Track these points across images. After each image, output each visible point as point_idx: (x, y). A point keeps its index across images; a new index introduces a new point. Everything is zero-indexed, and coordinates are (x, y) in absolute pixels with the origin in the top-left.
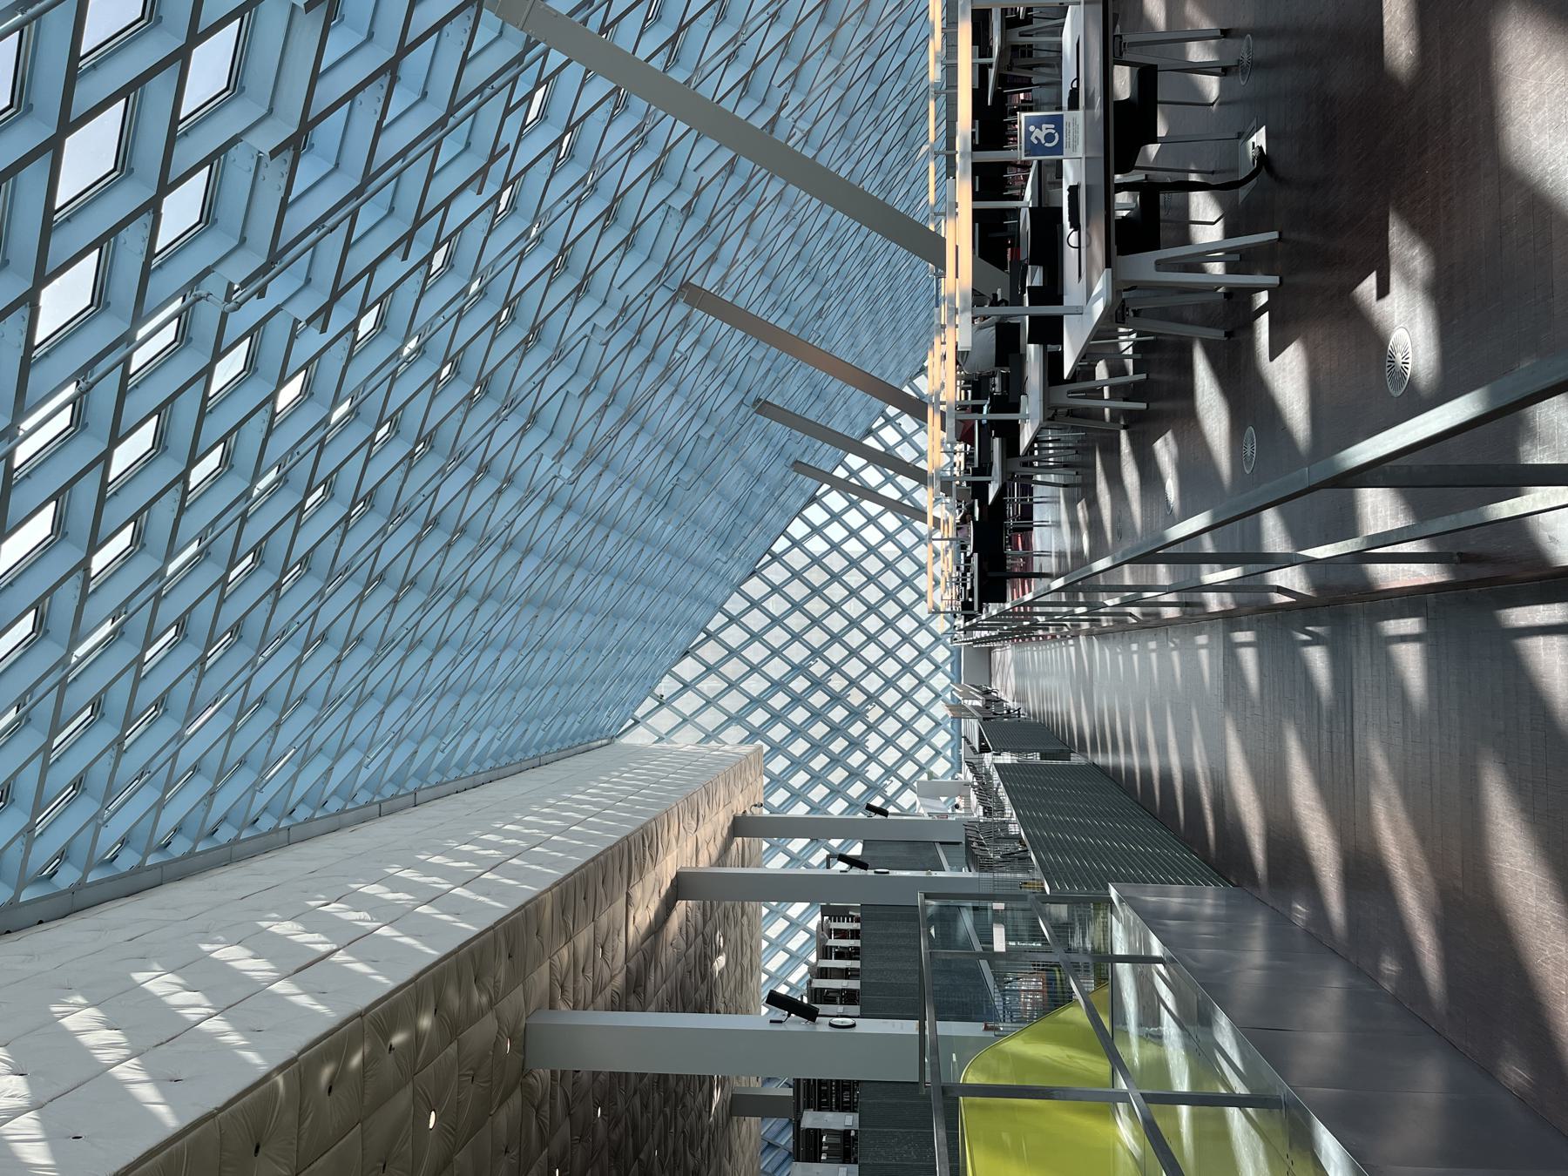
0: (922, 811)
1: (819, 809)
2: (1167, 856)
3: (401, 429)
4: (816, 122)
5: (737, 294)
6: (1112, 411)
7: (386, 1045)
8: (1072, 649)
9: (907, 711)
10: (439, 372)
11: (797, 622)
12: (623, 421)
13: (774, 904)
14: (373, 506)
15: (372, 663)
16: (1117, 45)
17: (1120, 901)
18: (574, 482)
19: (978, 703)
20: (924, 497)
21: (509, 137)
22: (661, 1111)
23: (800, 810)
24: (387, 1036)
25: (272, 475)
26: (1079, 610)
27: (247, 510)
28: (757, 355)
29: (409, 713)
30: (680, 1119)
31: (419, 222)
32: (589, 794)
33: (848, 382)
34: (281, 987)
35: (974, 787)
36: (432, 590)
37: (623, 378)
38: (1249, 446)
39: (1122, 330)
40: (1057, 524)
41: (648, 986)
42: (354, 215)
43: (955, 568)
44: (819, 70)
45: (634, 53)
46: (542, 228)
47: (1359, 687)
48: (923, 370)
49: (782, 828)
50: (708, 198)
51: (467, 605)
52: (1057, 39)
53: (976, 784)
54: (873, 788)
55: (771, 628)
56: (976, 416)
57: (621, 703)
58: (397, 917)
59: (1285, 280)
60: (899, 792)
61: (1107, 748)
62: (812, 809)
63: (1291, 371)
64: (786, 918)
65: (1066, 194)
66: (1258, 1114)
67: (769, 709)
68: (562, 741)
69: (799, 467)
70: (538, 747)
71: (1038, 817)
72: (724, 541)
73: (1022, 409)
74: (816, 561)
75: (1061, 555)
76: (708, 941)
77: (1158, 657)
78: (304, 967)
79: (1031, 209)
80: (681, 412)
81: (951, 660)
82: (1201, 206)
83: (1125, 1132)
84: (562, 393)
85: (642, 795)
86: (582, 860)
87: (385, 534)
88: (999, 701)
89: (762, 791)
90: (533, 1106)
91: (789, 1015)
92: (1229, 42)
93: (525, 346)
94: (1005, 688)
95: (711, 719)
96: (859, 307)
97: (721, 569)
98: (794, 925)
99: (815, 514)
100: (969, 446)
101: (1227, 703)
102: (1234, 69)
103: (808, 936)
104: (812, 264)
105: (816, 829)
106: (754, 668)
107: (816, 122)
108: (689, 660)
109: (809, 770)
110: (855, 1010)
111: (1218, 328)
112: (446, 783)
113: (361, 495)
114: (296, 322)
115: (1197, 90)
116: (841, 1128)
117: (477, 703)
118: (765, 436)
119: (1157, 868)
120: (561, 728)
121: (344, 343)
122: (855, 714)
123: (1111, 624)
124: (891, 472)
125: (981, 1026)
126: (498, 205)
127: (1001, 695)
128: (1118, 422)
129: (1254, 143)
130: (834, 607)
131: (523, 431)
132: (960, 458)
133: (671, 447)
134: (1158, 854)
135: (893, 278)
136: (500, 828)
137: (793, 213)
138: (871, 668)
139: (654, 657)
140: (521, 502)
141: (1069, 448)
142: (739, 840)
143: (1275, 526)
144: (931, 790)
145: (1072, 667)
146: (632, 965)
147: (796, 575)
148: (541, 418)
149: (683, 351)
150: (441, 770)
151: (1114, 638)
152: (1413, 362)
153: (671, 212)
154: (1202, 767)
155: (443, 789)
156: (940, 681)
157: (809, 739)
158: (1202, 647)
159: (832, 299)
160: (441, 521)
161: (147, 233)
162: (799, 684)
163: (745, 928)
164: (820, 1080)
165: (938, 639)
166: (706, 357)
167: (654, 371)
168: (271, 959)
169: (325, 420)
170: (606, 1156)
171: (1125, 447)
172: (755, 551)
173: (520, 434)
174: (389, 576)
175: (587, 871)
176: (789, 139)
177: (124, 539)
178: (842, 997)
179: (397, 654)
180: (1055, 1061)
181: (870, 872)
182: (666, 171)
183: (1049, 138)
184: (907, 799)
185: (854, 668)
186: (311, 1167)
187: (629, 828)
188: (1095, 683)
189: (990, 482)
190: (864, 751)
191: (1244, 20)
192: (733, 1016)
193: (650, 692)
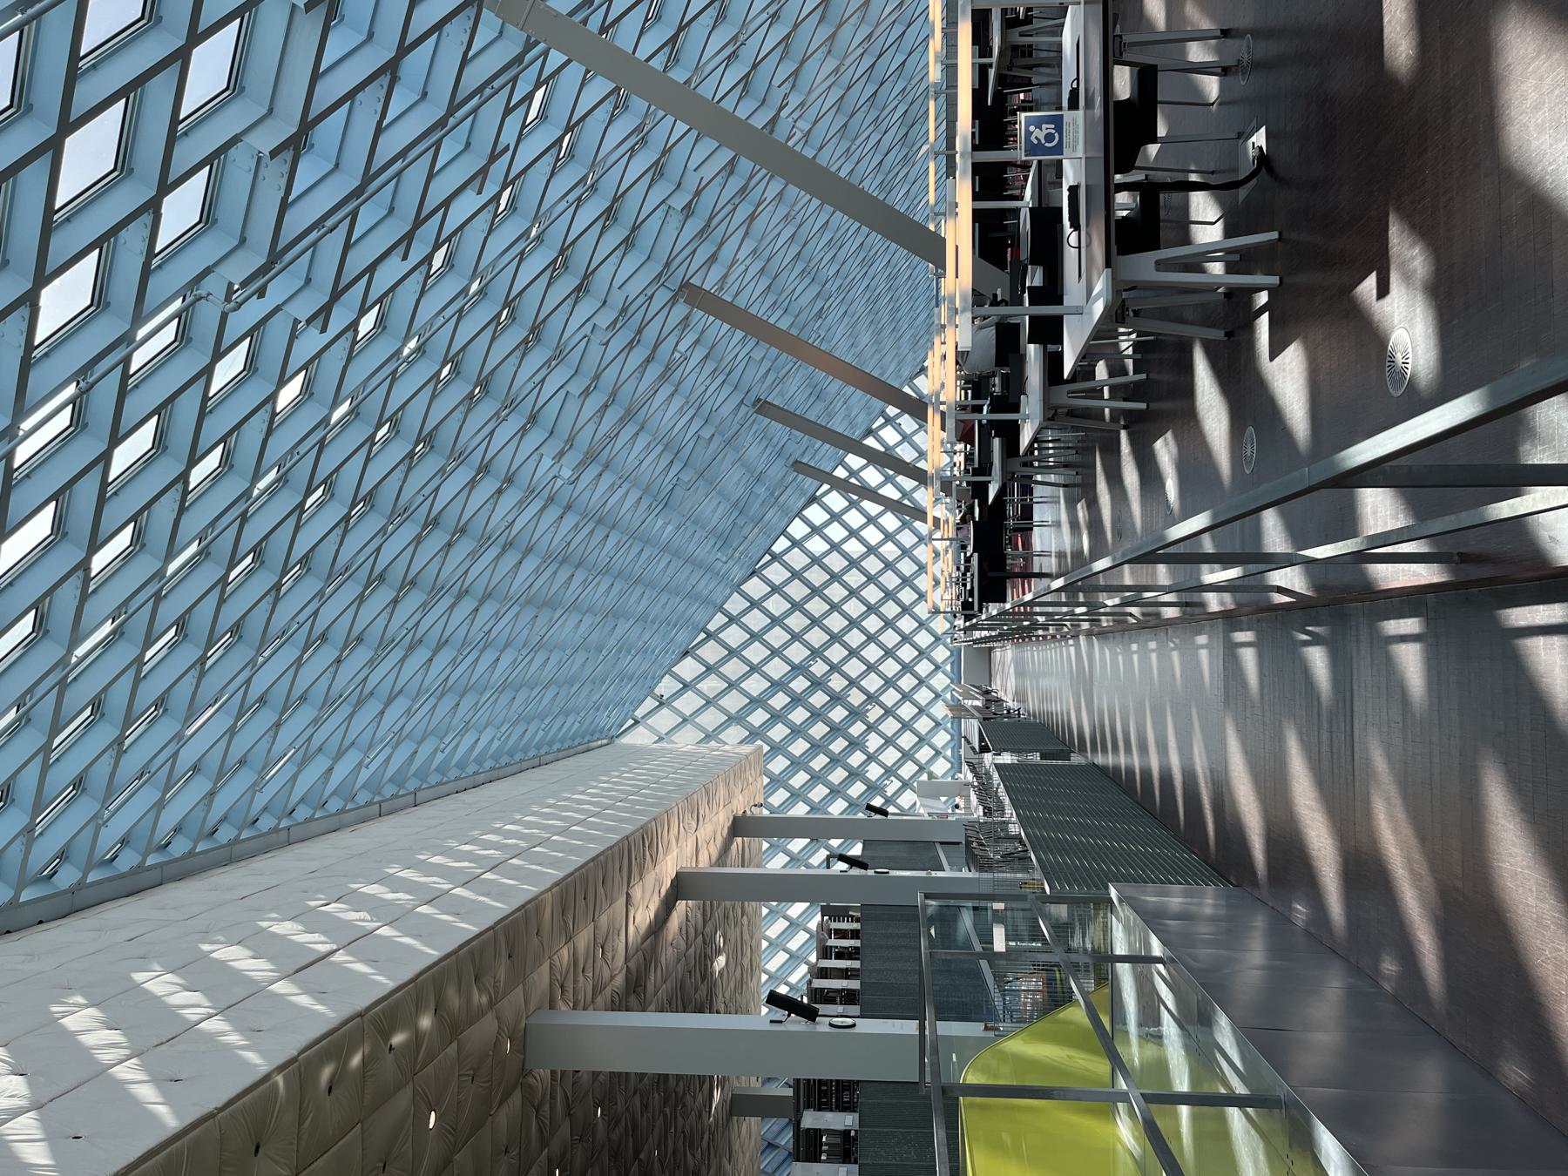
0: (922, 811)
1: (819, 809)
2: (1167, 856)
3: (401, 429)
4: (816, 122)
5: (737, 294)
6: (1112, 411)
7: (386, 1045)
8: (1072, 649)
9: (907, 711)
10: (439, 372)
11: (797, 622)
12: (623, 421)
13: (774, 904)
14: (373, 506)
15: (372, 663)
16: (1117, 45)
17: (1120, 901)
18: (574, 482)
19: (978, 703)
20: (924, 497)
21: (509, 137)
22: (661, 1111)
23: (800, 810)
24: (387, 1036)
25: (272, 475)
26: (1079, 610)
27: (247, 510)
28: (757, 355)
29: (409, 713)
30: (680, 1119)
31: (419, 222)
32: (589, 794)
33: (848, 382)
34: (281, 987)
35: (974, 787)
36: (432, 590)
37: (623, 378)
38: (1249, 446)
39: (1122, 330)
40: (1057, 524)
41: (648, 986)
42: (354, 215)
43: (955, 568)
44: (819, 70)
45: (634, 53)
46: (542, 228)
47: (1359, 687)
48: (923, 370)
49: (782, 828)
50: (708, 198)
51: (467, 605)
52: (1057, 39)
53: (976, 784)
54: (873, 788)
55: (771, 628)
56: (976, 416)
57: (621, 703)
58: (397, 917)
59: (1285, 280)
60: (899, 792)
61: (1107, 748)
62: (812, 809)
63: (1291, 371)
64: (786, 918)
65: (1066, 194)
66: (1258, 1114)
67: (769, 709)
68: (562, 741)
69: (799, 467)
70: (538, 747)
71: (1038, 817)
72: (724, 541)
73: (1022, 409)
74: (816, 561)
75: (1061, 555)
76: (708, 941)
77: (1158, 657)
78: (304, 967)
79: (1031, 209)
80: (681, 412)
81: (951, 660)
82: (1201, 206)
83: (1125, 1132)
84: (562, 393)
85: (642, 795)
86: (582, 860)
87: (385, 534)
88: (999, 701)
89: (762, 791)
90: (533, 1106)
91: (789, 1015)
92: (1229, 42)
93: (525, 346)
94: (1005, 688)
95: (711, 719)
96: (859, 307)
97: (721, 569)
98: (794, 925)
99: (815, 514)
100: (969, 446)
101: (1227, 703)
102: (1234, 69)
103: (808, 936)
104: (812, 264)
105: (816, 829)
106: (754, 668)
107: (816, 122)
108: (689, 660)
109: (809, 770)
110: (855, 1010)
111: (1218, 328)
112: (446, 783)
113: (361, 495)
114: (296, 322)
115: (1197, 90)
116: (841, 1128)
117: (477, 703)
118: (765, 436)
119: (1157, 868)
120: (561, 728)
121: (344, 343)
122: (855, 714)
123: (1111, 624)
124: (891, 472)
125: (981, 1026)
126: (498, 205)
127: (1001, 695)
128: (1118, 422)
129: (1254, 143)
130: (834, 607)
131: (523, 431)
132: (960, 458)
133: (671, 447)
134: (1158, 854)
135: (893, 278)
136: (500, 828)
137: (793, 213)
138: (871, 668)
139: (654, 657)
140: (521, 502)
141: (1069, 448)
142: (739, 840)
143: (1275, 526)
144: (931, 790)
145: (1072, 667)
146: (632, 965)
147: (796, 575)
148: (541, 418)
149: (683, 351)
150: (441, 770)
151: (1114, 638)
152: (1413, 362)
153: (671, 212)
154: (1202, 767)
155: (443, 789)
156: (940, 681)
157: (809, 739)
158: (1202, 647)
159: (832, 299)
160: (441, 521)
161: (147, 233)
162: (799, 684)
163: (745, 928)
164: (820, 1080)
165: (938, 639)
166: (706, 357)
167: (654, 371)
168: (271, 959)
169: (325, 420)
170: (606, 1156)
171: (1125, 447)
172: (755, 551)
173: (520, 434)
174: (389, 576)
175: (587, 871)
176: (789, 139)
177: (124, 539)
178: (842, 997)
179: (397, 654)
180: (1055, 1061)
181: (870, 872)
182: (666, 171)
183: (1049, 138)
184: (907, 799)
185: (854, 668)
186: (311, 1167)
187: (629, 828)
188: (1095, 683)
189: (990, 482)
190: (864, 751)
191: (1244, 20)
192: (733, 1016)
193: (650, 692)
